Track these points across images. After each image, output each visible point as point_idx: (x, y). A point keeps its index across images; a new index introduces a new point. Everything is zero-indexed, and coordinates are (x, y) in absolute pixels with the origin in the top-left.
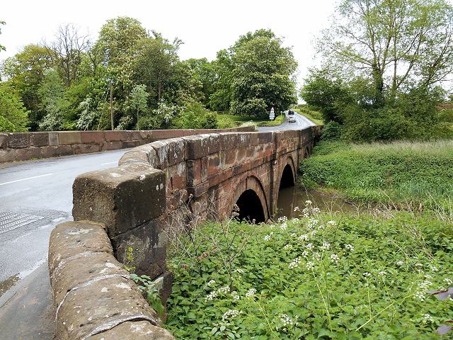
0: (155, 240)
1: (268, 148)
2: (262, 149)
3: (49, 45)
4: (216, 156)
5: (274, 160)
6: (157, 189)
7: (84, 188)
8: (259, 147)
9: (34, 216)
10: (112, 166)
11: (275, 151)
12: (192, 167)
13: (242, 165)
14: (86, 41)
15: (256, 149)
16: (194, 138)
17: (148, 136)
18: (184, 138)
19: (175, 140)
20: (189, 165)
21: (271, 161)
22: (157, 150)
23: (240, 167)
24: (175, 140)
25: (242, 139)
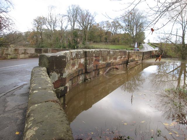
8: (120, 57)
15: (119, 57)
18: (83, 50)
22: (71, 52)
23: (110, 63)
25: (111, 52)
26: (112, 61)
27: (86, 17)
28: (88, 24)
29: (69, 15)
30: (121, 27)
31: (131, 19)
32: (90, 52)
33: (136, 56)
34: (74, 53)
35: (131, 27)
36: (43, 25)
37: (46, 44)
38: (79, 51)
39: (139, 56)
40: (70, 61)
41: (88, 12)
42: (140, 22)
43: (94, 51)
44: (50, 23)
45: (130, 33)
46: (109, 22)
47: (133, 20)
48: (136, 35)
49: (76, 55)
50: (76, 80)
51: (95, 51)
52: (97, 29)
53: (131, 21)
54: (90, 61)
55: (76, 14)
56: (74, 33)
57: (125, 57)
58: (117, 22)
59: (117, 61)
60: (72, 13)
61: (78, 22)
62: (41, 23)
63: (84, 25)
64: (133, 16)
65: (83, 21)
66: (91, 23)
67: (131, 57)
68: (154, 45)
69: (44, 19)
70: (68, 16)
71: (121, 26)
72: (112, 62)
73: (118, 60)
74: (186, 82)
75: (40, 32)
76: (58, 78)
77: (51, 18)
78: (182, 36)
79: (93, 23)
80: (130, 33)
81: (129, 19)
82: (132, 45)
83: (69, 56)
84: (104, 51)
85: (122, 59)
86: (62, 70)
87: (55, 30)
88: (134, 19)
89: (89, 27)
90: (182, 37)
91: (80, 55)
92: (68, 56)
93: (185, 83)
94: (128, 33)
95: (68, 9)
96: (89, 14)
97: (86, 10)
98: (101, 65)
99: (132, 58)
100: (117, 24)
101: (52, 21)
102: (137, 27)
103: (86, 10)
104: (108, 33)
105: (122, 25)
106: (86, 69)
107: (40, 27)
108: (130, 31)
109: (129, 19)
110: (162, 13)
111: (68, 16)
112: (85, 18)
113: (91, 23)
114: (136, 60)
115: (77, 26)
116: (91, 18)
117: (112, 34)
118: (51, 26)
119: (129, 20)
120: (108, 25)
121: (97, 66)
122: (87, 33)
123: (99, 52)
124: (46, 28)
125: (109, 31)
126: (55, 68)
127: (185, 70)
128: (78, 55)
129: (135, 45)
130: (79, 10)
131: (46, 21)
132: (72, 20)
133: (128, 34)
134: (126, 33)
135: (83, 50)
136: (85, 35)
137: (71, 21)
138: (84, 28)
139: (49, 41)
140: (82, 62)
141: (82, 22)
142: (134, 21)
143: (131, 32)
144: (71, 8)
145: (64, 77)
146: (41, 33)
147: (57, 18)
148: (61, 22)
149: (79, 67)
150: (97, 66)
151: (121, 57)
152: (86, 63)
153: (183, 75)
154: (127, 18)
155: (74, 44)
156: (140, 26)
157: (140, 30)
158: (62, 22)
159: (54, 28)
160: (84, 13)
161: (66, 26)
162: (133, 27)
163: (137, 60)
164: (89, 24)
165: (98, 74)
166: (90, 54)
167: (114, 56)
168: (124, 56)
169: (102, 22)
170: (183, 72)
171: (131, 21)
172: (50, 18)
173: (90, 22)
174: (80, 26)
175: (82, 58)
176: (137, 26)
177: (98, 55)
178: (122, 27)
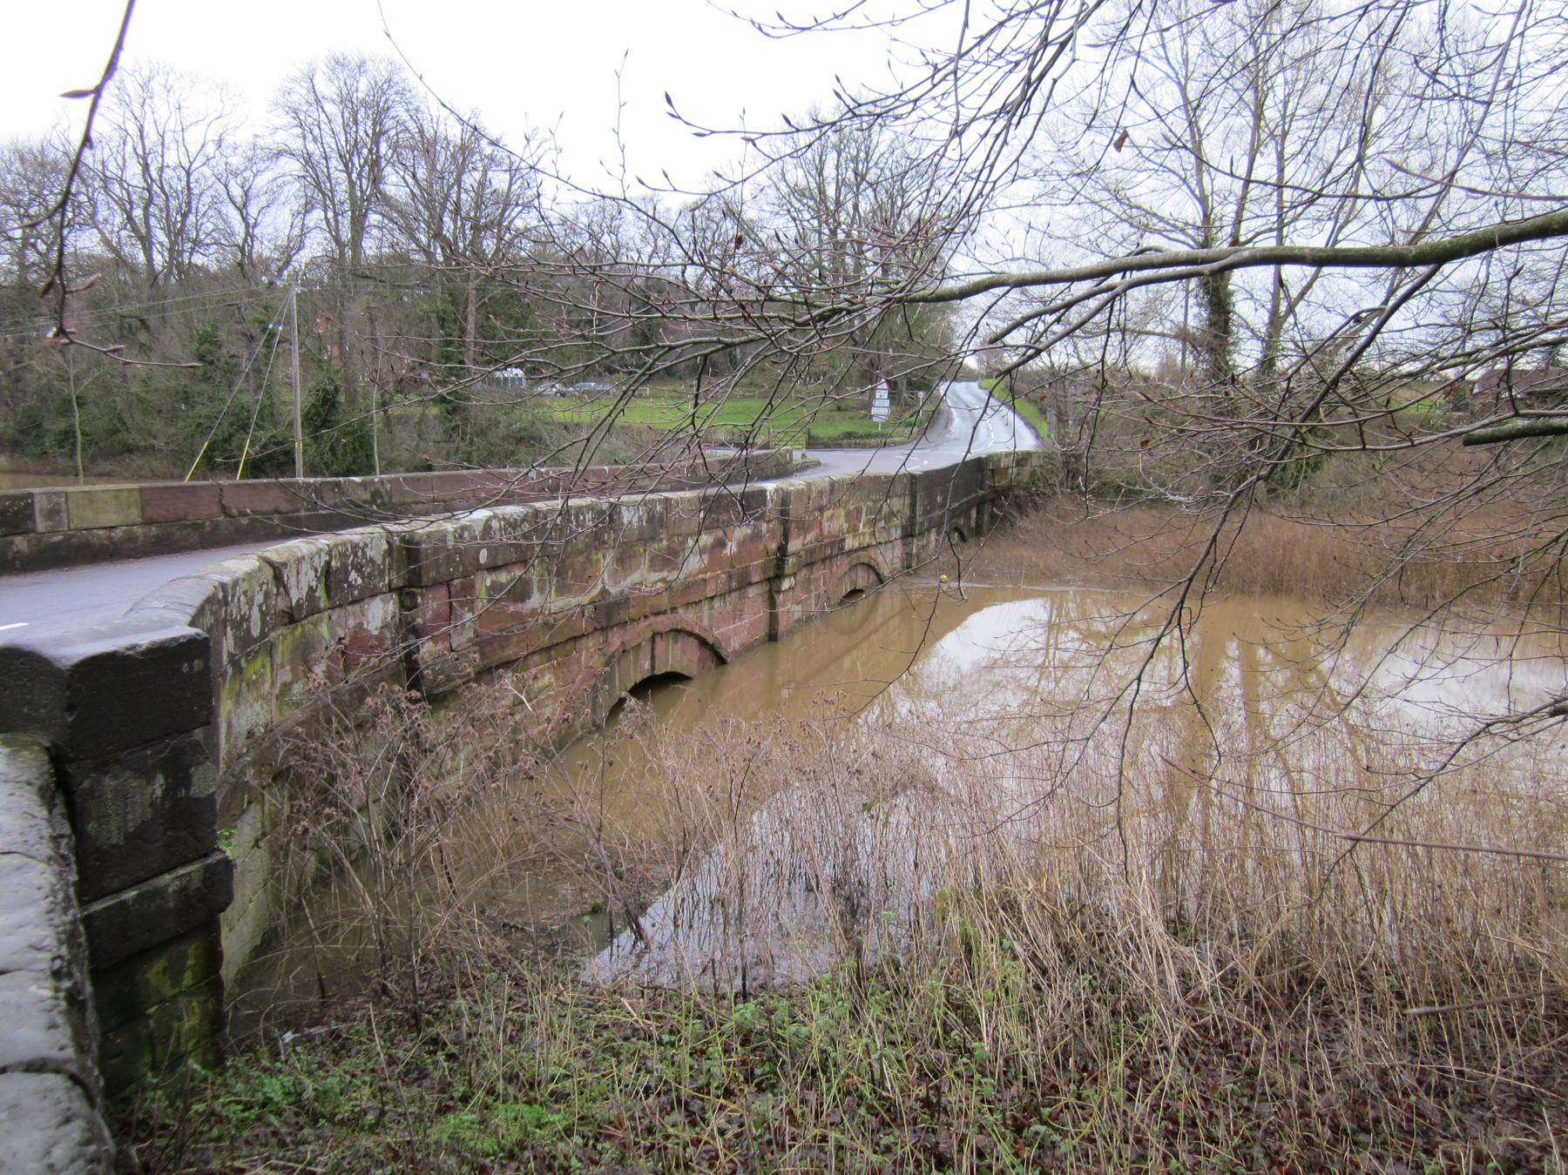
0: (179, 775)
2: (720, 544)
4: (518, 572)
5: (779, 576)
11: (782, 549)
12: (416, 606)
13: (628, 599)
14: (213, 135)
17: (376, 495)
20: (408, 603)
23: (622, 602)
25: (627, 516)
31: (838, 189)
32: (450, 543)
38: (355, 546)
40: (263, 635)
43: (479, 529)
44: (138, 213)
51: (489, 520)
55: (369, 136)
60: (339, 129)
63: (438, 235)
72: (634, 587)
77: (146, 167)
83: (259, 598)
87: (188, 274)
91: (359, 570)
92: (250, 603)
101: (159, 201)
110: (965, 212)
114: (850, 543)
116: (499, 180)
118: (146, 242)
119: (822, 192)
128: (347, 574)
132: (342, 192)
147: (202, 173)
148: (242, 209)
154: (803, 183)
158: (253, 210)
167: (654, 538)
172: (134, 173)
173: (491, 211)
175: (373, 596)
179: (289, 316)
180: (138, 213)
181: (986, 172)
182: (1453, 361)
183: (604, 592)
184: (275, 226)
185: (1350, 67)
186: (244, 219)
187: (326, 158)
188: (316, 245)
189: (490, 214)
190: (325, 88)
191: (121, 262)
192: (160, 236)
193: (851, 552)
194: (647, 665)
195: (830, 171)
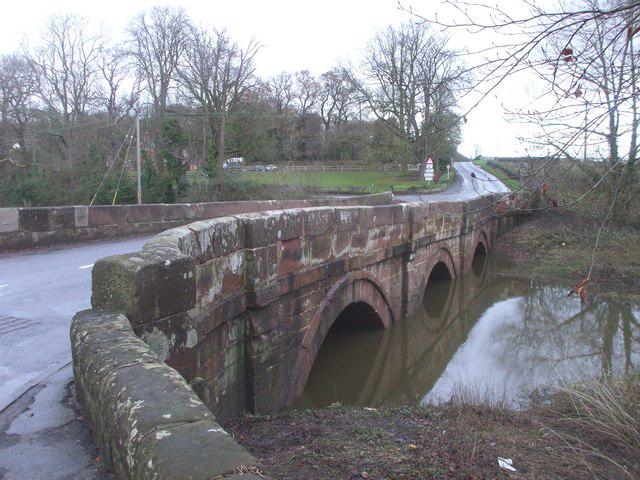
1: (394, 233)
3: (34, 55)
6: (185, 277)
7: (103, 274)
8: (377, 231)
9: (292, 176)
10: (129, 252)
14: (97, 46)
15: (371, 233)
16: (254, 216)
18: (238, 216)
19: (224, 220)
21: (402, 254)
22: (196, 234)
23: (341, 263)
24: (224, 220)
25: (343, 217)
26: (349, 250)
27: (218, 57)
28: (227, 86)
29: (143, 50)
30: (361, 94)
31: (402, 64)
33: (439, 223)
34: (206, 233)
35: (406, 97)
36: (28, 93)
37: (45, 177)
39: (448, 220)
41: (225, 36)
42: (440, 72)
44: (60, 86)
45: (401, 118)
46: (311, 75)
47: (412, 67)
48: (427, 125)
49: (214, 240)
50: (216, 346)
51: (282, 216)
52: (264, 106)
53: (402, 71)
54: (264, 264)
55: (169, 40)
56: (167, 129)
57: (397, 232)
58: (346, 75)
59: (366, 250)
61: (182, 80)
62: (19, 86)
63: (207, 91)
64: (411, 49)
65: (202, 75)
66: (236, 84)
67: (419, 230)
68: (499, 167)
69: (34, 70)
70: (140, 55)
71: (363, 91)
72: (346, 255)
73: (370, 243)
74: (634, 357)
75: (13, 126)
76: (170, 350)
77: (65, 63)
78: (608, 132)
79: (245, 84)
80: (401, 118)
81: (393, 61)
82: (412, 169)
84: (316, 212)
85: (387, 238)
86: (183, 317)
88: (413, 61)
89: (229, 99)
90: (608, 136)
93: (629, 362)
94: (392, 120)
95: (137, 25)
96: (229, 46)
97: (214, 30)
98: (309, 273)
99: (421, 234)
100: (344, 83)
101: (71, 78)
102: (427, 96)
103: (214, 30)
104: (307, 121)
105: (364, 87)
106: (251, 295)
107: (14, 103)
108: (398, 109)
109: (393, 61)
111: (140, 55)
112: (212, 61)
113: (236, 84)
114: (438, 237)
115: (176, 93)
116: (236, 63)
117: (327, 124)
118: (63, 98)
119: (394, 66)
120: (306, 86)
121: (291, 278)
122: (223, 126)
123: (299, 220)
124: (42, 106)
125: (313, 111)
126: (157, 311)
127: (629, 318)
129: (423, 169)
130: (186, 30)
131: (42, 77)
132: (156, 72)
133: (391, 121)
134: (382, 119)
135: (238, 216)
136: (216, 134)
137: (150, 75)
138: (210, 103)
139: (57, 165)
140: (234, 268)
141: (200, 81)
142: (416, 70)
143: (406, 117)
144: (149, 22)
145: (191, 347)
146: (21, 129)
147: (93, 65)
149: (223, 291)
150: (291, 278)
151: (382, 234)
152: (249, 269)
153: (620, 333)
154: (384, 60)
155: (166, 174)
156: (438, 90)
157: (441, 107)
158: (115, 82)
159: (77, 104)
160: (207, 40)
161: (129, 98)
162: (413, 95)
163: (442, 236)
164: (231, 86)
165: (299, 310)
166: (266, 231)
168: (391, 228)
169: (284, 79)
170: (620, 323)
171: (402, 71)
172: (59, 65)
174: (192, 95)
176: (425, 89)
177: (292, 231)
178: (368, 97)
179: (136, 132)
180: (60, 86)
181: (561, 25)
182: (541, 37)
183: (333, 256)
184: (126, 87)
185: (573, 21)
186: (111, 85)
187: (149, 55)
188: (146, 99)
189: (233, 80)
190: (149, 22)
191: (52, 110)
192: (70, 96)
193: (439, 241)
194: (351, 298)
195: (397, 54)
